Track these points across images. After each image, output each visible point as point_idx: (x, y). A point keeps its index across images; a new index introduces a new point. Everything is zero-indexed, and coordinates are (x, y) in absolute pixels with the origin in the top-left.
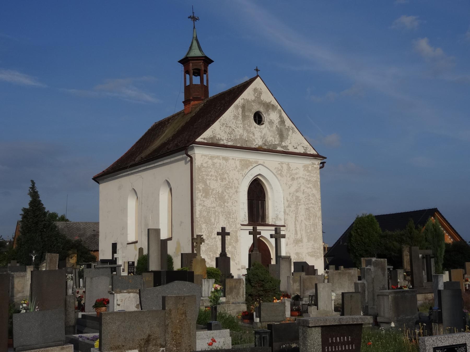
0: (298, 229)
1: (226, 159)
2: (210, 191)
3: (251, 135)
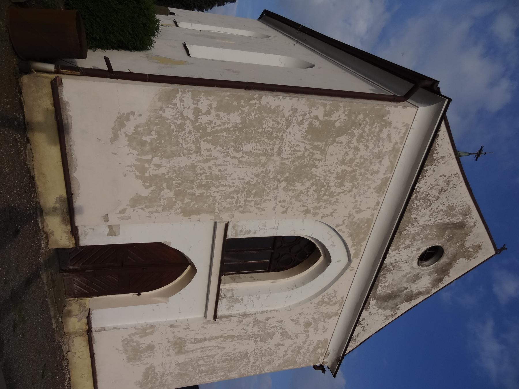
0: (207, 344)
1: (385, 182)
2: (322, 144)
3: (407, 242)
